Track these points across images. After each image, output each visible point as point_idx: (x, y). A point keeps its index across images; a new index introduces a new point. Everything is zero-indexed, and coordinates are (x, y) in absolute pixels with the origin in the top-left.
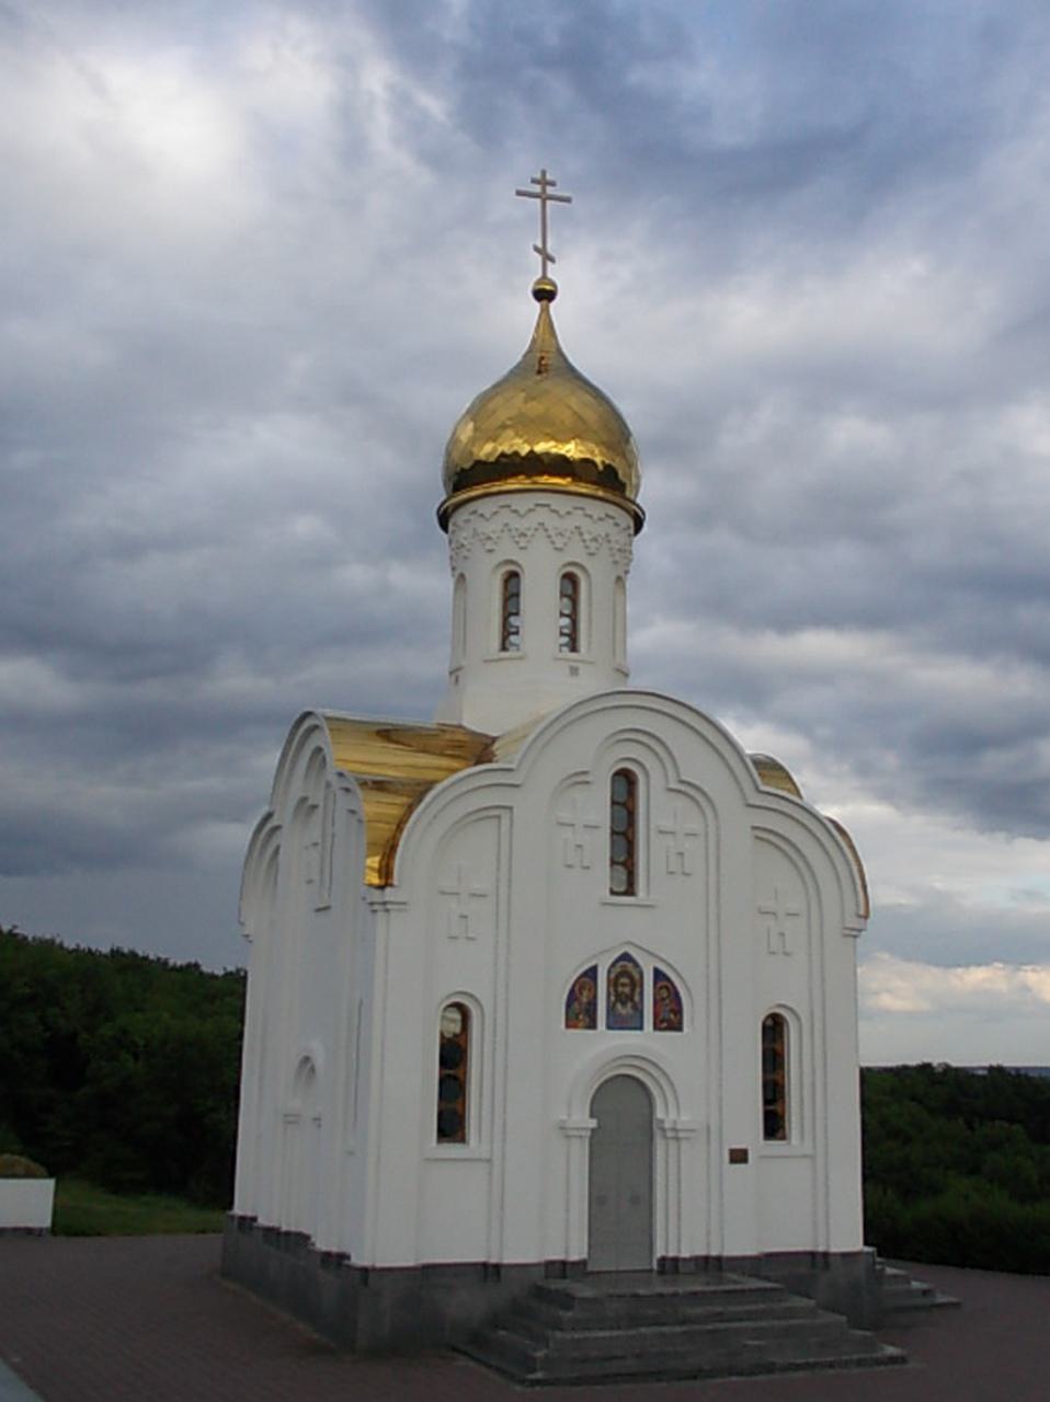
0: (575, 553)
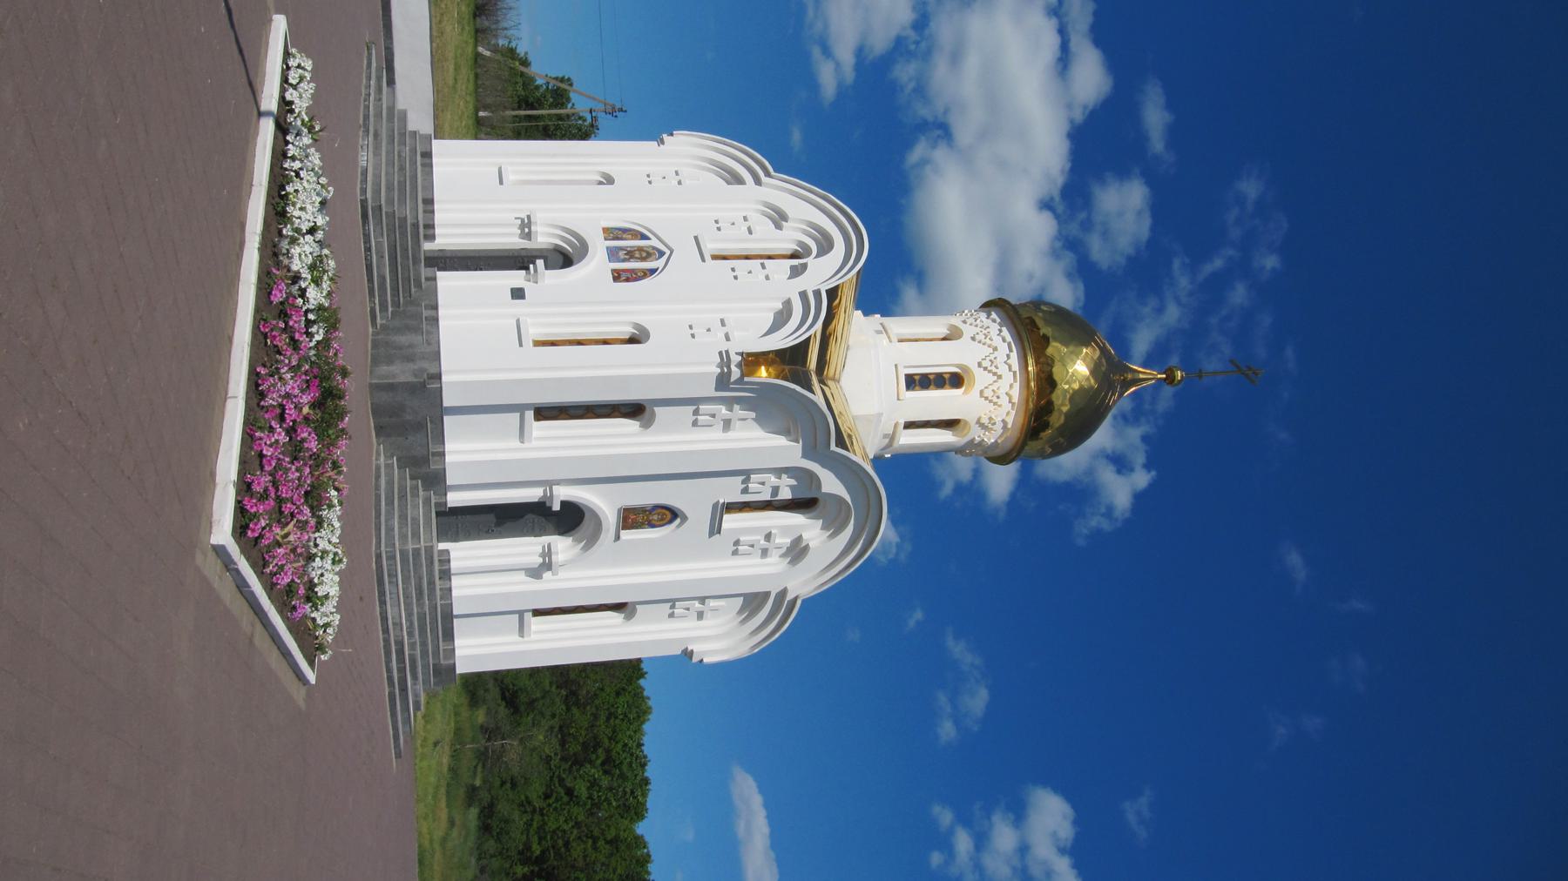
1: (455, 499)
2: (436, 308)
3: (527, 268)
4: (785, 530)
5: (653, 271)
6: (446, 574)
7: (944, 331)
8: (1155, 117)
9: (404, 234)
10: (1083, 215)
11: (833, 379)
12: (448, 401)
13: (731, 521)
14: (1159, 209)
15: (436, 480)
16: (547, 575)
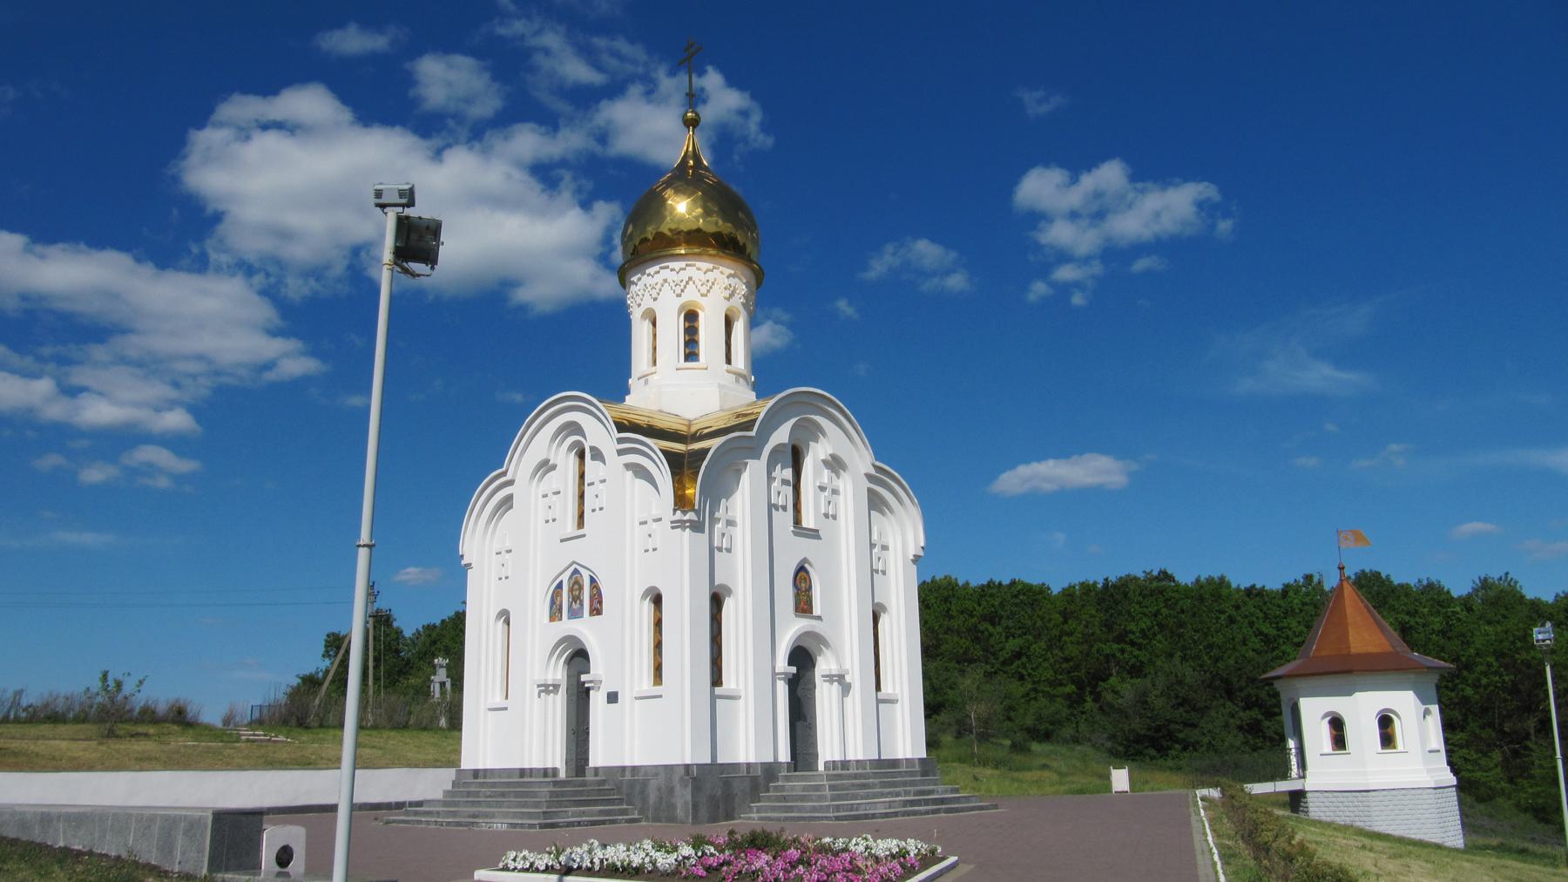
1: (784, 756)
2: (623, 768)
3: (588, 689)
4: (817, 474)
5: (593, 580)
6: (845, 764)
7: (647, 325)
8: (352, 41)
9: (563, 794)
10: (451, 123)
11: (689, 426)
12: (706, 759)
13: (808, 521)
14: (447, 45)
15: (770, 771)
16: (848, 679)
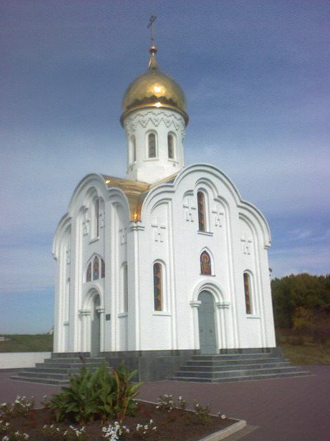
0: (172, 128)
5: (102, 261)
